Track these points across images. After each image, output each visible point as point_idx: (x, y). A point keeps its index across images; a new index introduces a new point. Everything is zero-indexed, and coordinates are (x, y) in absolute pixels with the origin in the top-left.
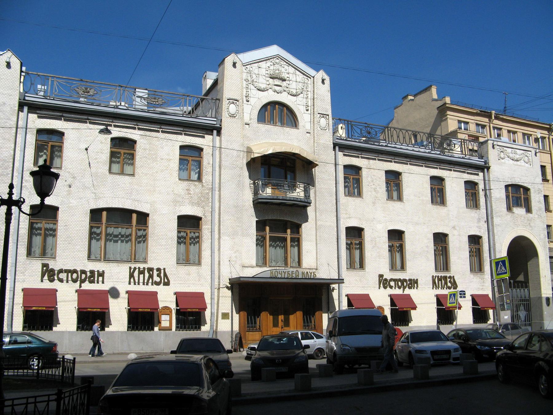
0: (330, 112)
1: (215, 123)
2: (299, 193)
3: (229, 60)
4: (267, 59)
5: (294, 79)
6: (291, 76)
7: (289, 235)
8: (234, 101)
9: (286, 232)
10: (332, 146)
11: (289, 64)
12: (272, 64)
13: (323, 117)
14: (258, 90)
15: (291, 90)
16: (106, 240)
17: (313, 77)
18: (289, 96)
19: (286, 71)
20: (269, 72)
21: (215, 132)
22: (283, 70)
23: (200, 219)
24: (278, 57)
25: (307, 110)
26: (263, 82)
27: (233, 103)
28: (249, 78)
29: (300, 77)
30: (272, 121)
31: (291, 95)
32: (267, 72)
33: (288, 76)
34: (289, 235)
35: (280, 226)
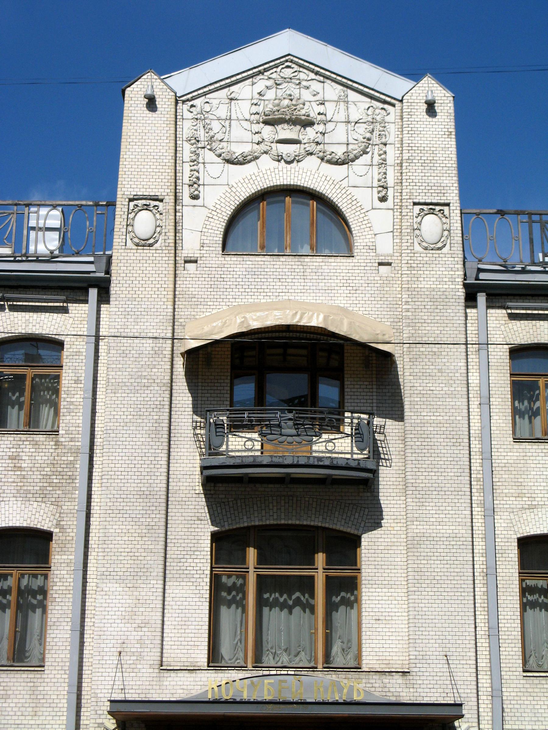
0: (453, 196)
1: (91, 268)
2: (337, 446)
3: (135, 95)
4: (259, 71)
5: (342, 116)
6: (330, 109)
7: (320, 569)
8: (148, 202)
9: (311, 562)
10: (461, 293)
11: (325, 75)
12: (270, 83)
13: (432, 212)
14: (229, 161)
15: (329, 149)
16: (261, 603)
17: (401, 101)
18: (325, 165)
19: (316, 95)
20: (260, 109)
21: (93, 293)
22: (306, 95)
23: (46, 536)
24: (286, 60)
25: (383, 199)
26: (240, 141)
27: (146, 207)
28: (202, 135)
29: (359, 106)
30: (273, 244)
31: (329, 162)
32: (254, 109)
33: (321, 109)
34: (320, 569)
35: (288, 544)
